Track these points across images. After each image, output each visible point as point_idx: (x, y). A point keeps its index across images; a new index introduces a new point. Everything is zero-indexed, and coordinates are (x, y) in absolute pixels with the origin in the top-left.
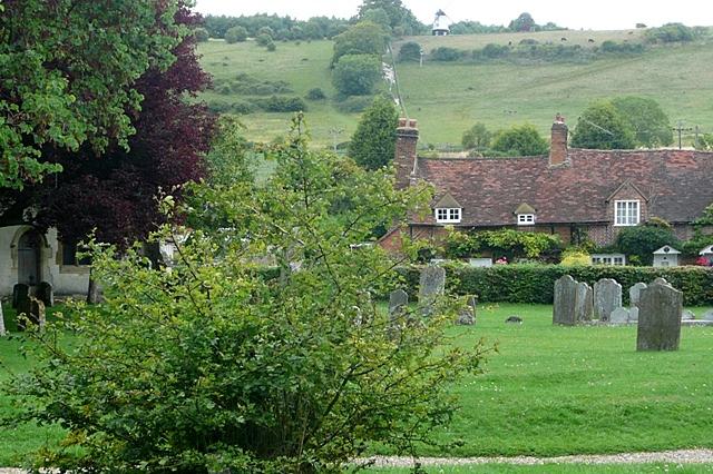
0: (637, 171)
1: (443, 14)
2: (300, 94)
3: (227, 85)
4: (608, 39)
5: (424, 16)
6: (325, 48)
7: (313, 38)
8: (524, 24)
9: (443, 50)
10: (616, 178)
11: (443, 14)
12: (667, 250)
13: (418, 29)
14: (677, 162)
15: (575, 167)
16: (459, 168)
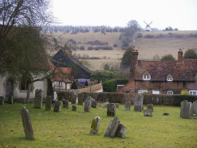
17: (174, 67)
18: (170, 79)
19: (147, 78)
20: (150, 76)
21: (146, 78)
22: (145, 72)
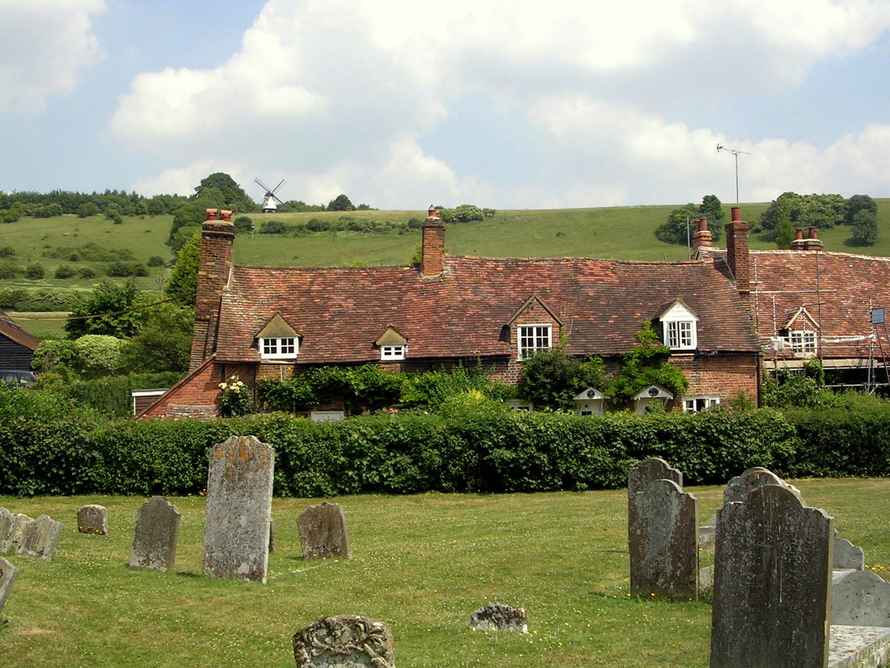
0: (541, 285)
1: (272, 195)
2: (143, 259)
3: (76, 252)
4: (412, 217)
5: (256, 196)
6: (166, 222)
7: (157, 213)
8: (342, 203)
9: (271, 224)
10: (513, 295)
11: (272, 195)
12: (591, 394)
13: (251, 207)
14: (592, 274)
15: (457, 279)
16: (294, 280)
17: (406, 292)
18: (393, 351)
19: (284, 350)
20: (296, 341)
21: (274, 351)
22: (269, 320)
